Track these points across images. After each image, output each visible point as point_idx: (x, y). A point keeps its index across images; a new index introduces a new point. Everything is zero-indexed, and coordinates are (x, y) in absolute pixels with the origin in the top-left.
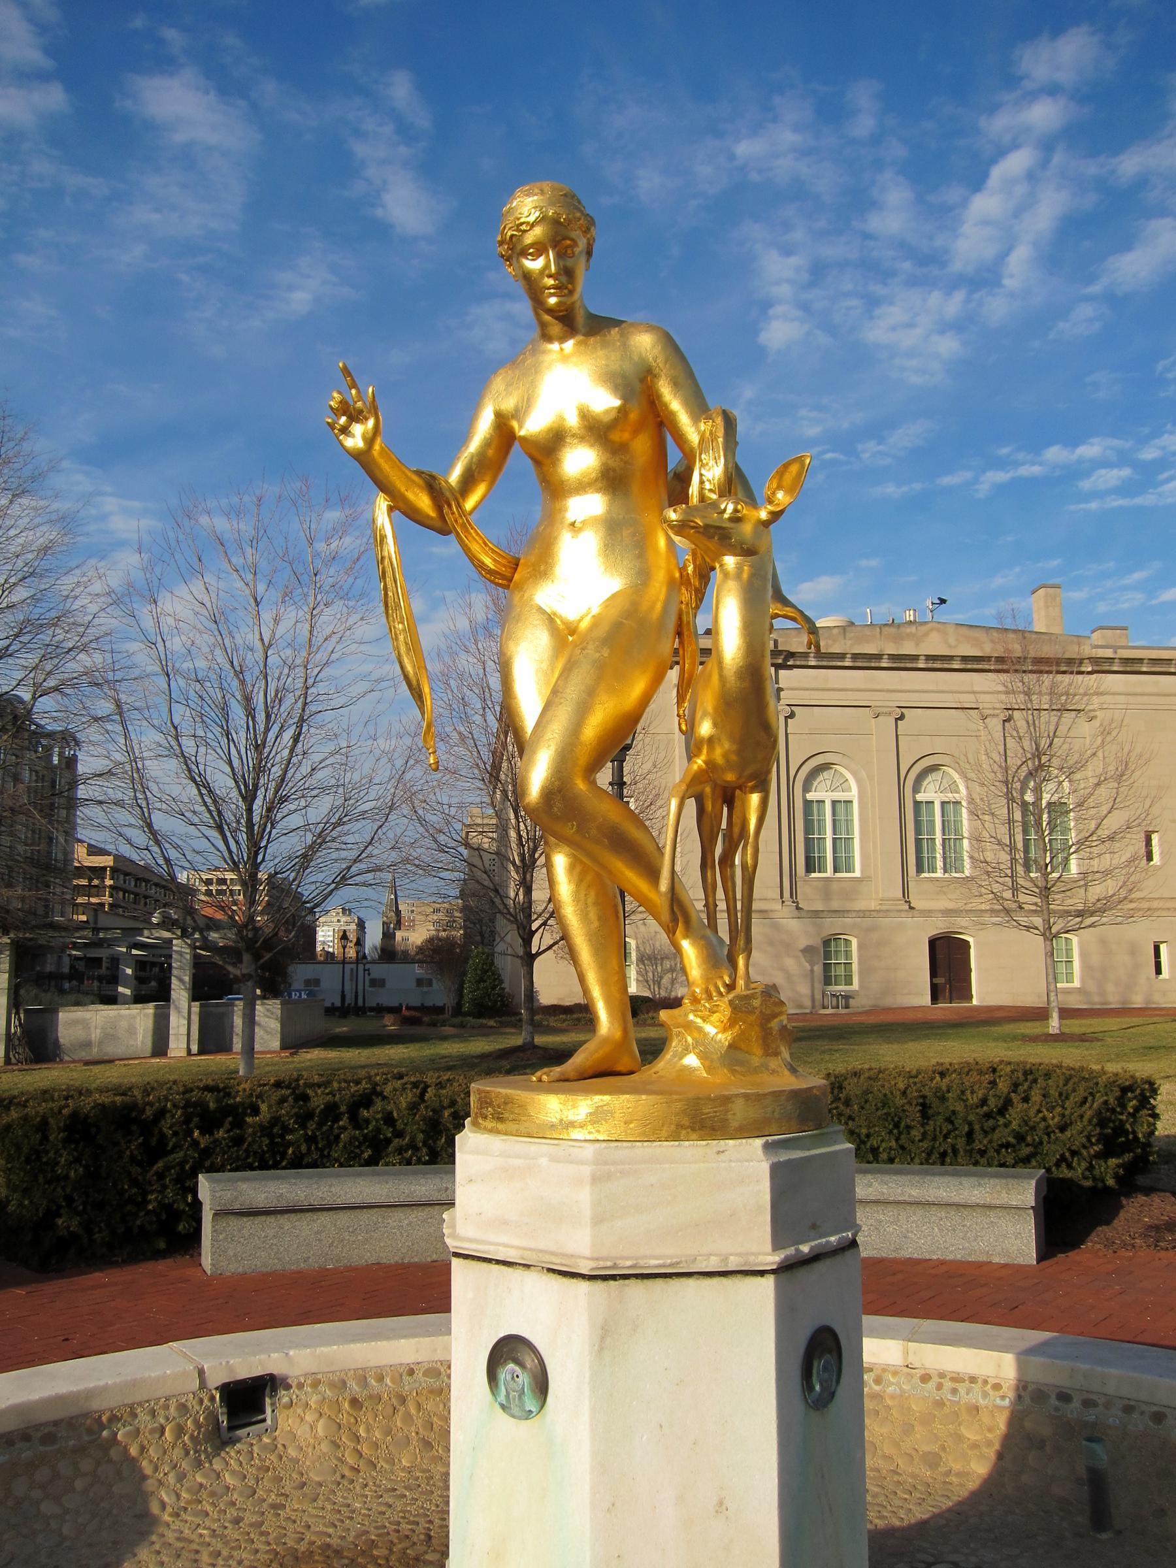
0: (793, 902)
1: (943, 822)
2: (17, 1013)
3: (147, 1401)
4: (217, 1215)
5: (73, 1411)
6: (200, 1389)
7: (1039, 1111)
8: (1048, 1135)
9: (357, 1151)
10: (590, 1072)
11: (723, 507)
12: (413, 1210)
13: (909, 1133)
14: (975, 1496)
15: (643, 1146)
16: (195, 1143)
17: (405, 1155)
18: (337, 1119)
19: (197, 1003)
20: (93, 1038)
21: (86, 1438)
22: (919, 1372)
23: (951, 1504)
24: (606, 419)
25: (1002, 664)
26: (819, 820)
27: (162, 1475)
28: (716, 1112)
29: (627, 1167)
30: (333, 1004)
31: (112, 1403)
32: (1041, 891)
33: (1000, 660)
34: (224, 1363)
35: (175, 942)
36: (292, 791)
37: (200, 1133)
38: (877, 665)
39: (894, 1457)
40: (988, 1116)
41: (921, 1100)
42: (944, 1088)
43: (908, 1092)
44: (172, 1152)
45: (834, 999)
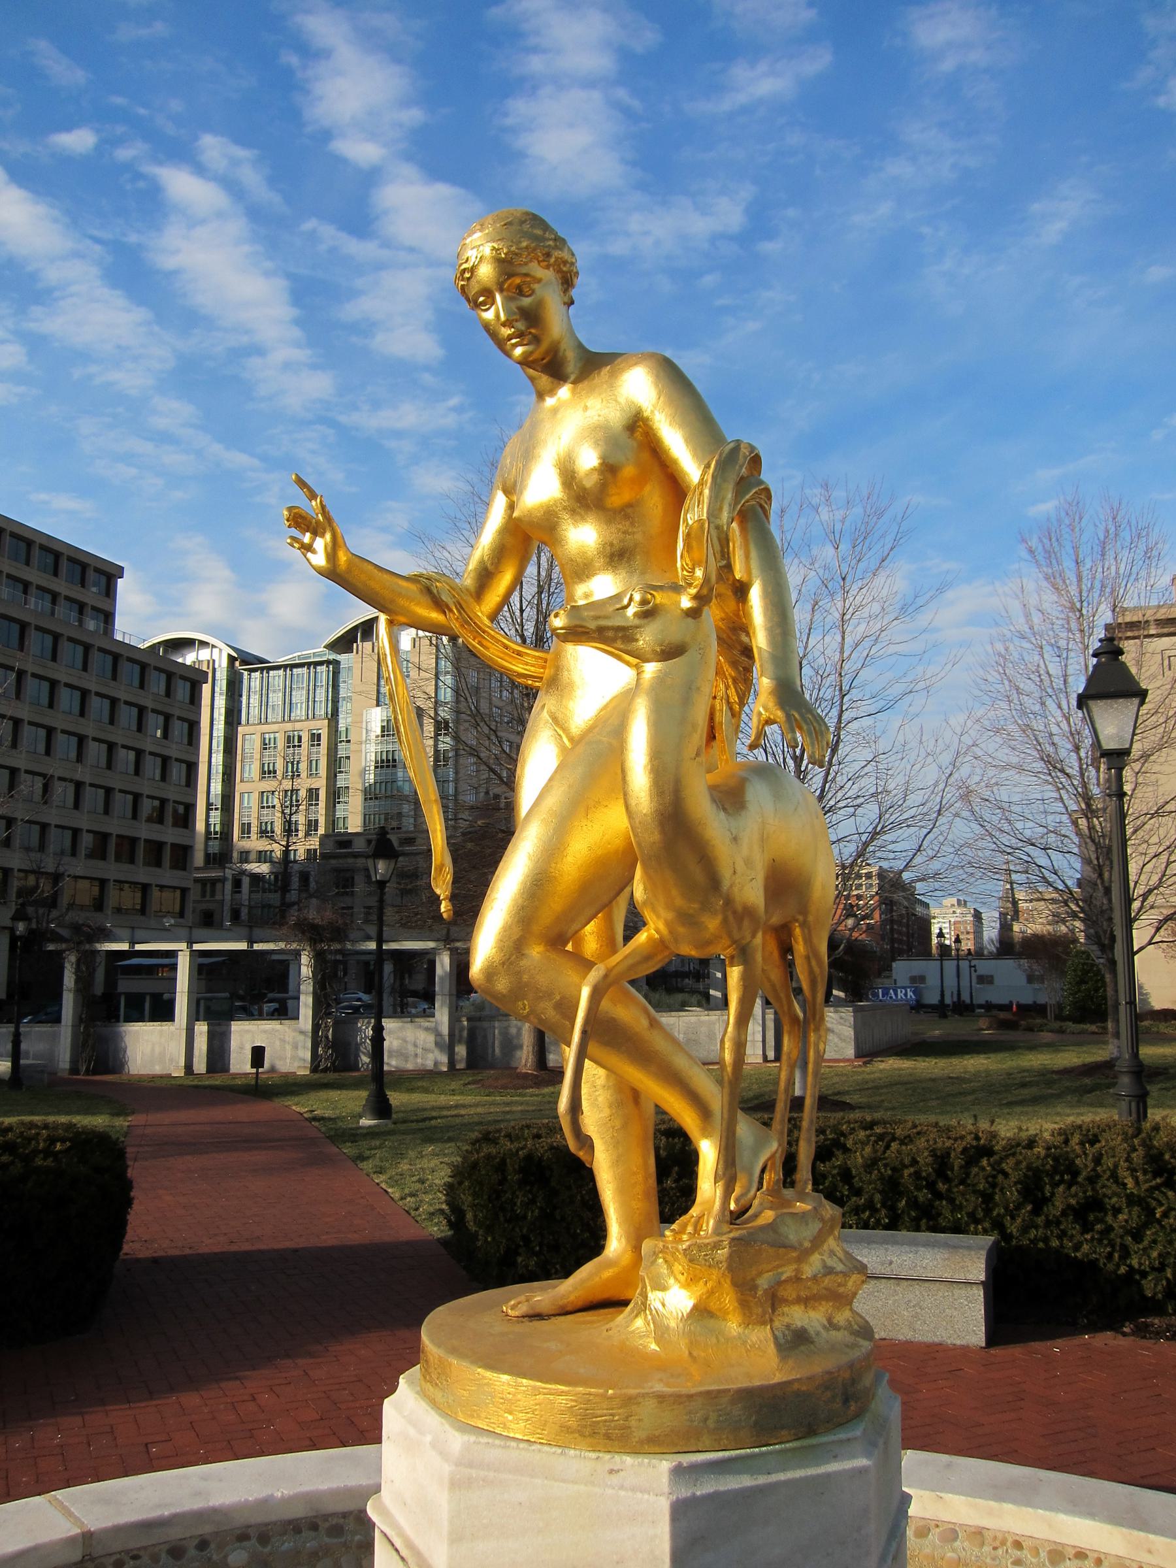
10: (580, 1304)
15: (518, 1448)
17: (862, 1216)
29: (491, 1474)
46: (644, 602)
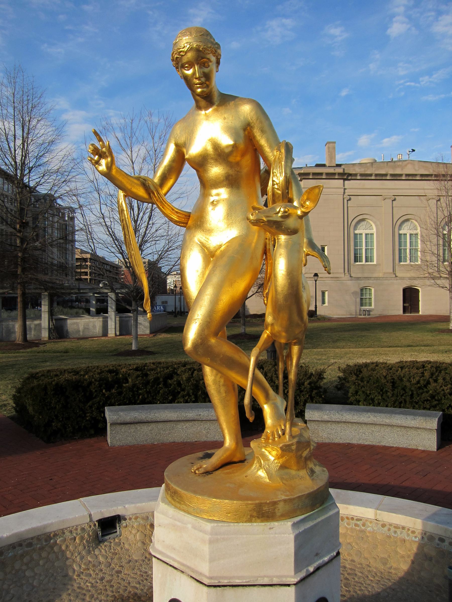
0: (349, 274)
1: (410, 242)
2: (52, 320)
3: (69, 527)
4: (111, 424)
5: (39, 533)
6: (90, 522)
7: (441, 387)
8: (445, 396)
9: (167, 397)
10: (220, 466)
11: (278, 210)
12: (187, 422)
13: (387, 393)
14: (402, 579)
15: (234, 525)
16: (104, 394)
18: (159, 384)
19: (118, 317)
20: (80, 330)
21: (44, 543)
22: (381, 523)
23: (390, 584)
24: (227, 151)
25: (437, 177)
26: (360, 242)
27: (74, 557)
28: (269, 509)
29: (226, 536)
30: (172, 310)
31: (55, 529)
32: (449, 273)
33: (436, 176)
34: (99, 511)
35: (109, 294)
36: (149, 238)
37: (105, 391)
38: (385, 178)
39: (369, 559)
40: (420, 388)
41: (392, 381)
42: (402, 376)
43: (387, 376)
44: (95, 398)
45: (364, 312)
46: (285, 212)
